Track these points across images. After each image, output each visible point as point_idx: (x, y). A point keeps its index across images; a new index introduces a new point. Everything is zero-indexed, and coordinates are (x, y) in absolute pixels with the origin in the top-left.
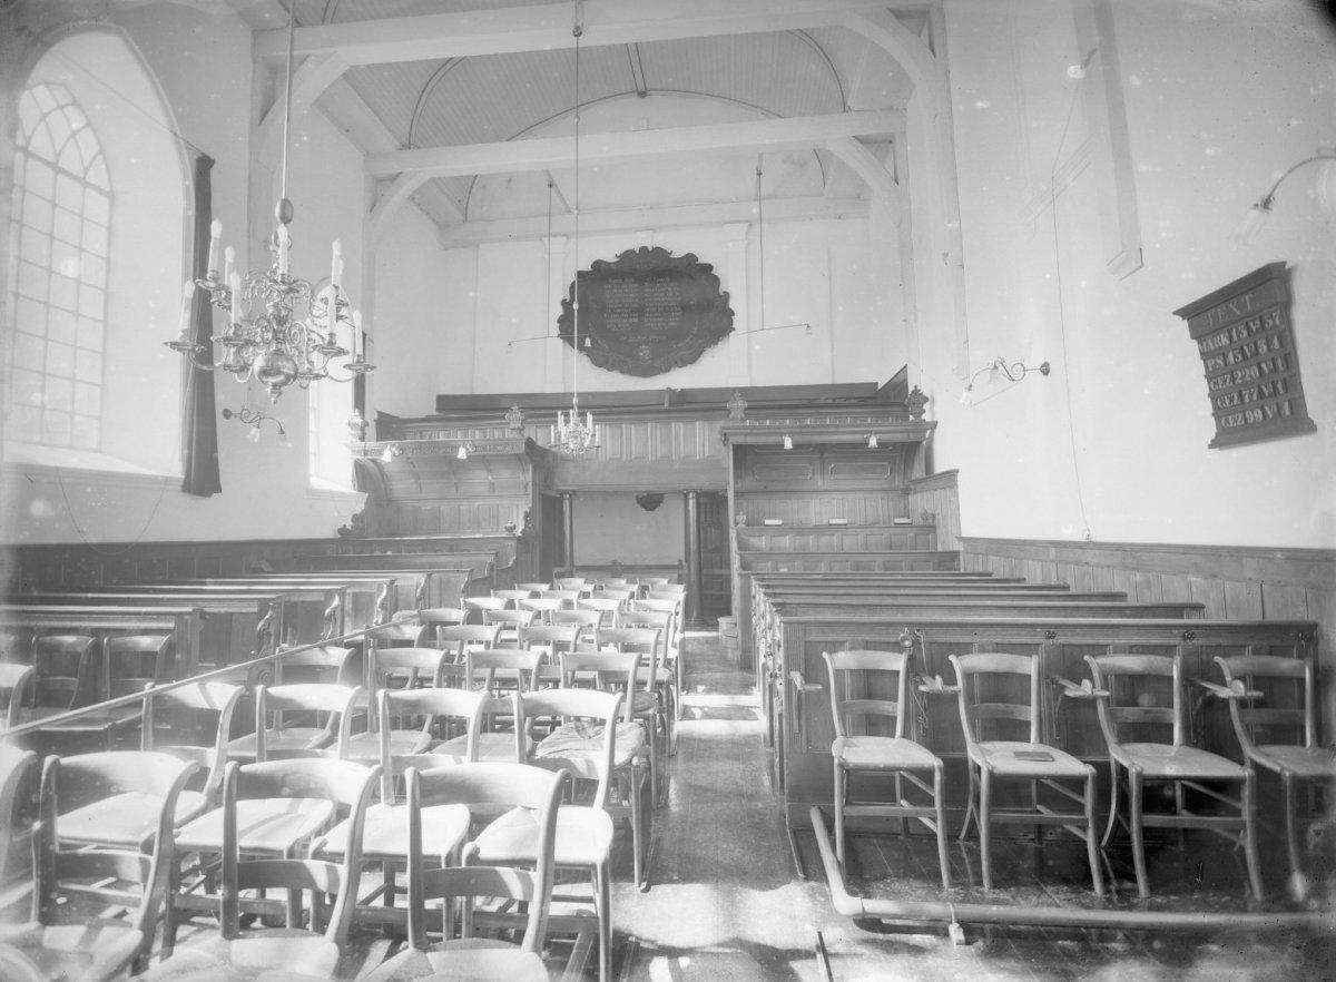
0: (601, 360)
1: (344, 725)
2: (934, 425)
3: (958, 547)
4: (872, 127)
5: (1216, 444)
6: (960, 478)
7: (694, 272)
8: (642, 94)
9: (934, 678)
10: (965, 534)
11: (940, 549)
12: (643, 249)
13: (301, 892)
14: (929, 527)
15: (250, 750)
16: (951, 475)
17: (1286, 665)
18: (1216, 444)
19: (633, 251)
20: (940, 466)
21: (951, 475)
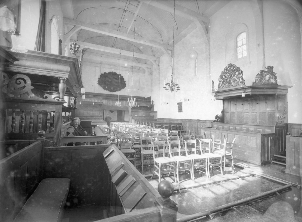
0: (105, 88)
1: (164, 155)
2: (154, 105)
3: (157, 119)
4: (149, 67)
5: (178, 112)
6: (158, 112)
7: (122, 79)
8: (113, 47)
9: (85, 92)
10: (158, 118)
11: (154, 119)
12: (113, 72)
13: (275, 132)
14: (153, 117)
15: (231, 151)
16: (156, 112)
17: (180, 126)
18: (178, 112)
19: (111, 72)
20: (155, 110)
21: (156, 112)
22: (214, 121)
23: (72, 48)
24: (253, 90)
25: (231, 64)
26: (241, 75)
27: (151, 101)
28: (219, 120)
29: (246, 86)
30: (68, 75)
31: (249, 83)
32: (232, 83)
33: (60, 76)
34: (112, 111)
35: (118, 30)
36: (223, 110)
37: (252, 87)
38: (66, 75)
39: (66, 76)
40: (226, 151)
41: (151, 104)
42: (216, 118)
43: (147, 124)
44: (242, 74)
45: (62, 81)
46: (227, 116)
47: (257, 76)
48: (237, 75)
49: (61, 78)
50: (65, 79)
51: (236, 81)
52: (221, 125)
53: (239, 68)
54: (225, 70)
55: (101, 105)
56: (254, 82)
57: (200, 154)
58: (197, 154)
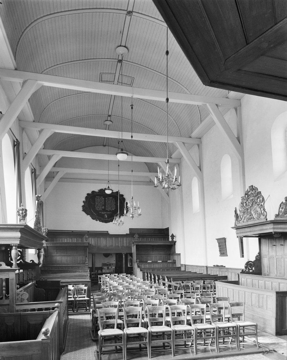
10: (181, 263)
16: (179, 254)
22: (243, 272)
23: (19, 215)
24: (276, 226)
25: (252, 186)
26: (262, 204)
27: (170, 235)
28: (252, 269)
29: (268, 220)
30: (19, 241)
31: (271, 217)
32: (253, 215)
33: (12, 243)
34: (107, 255)
35: (113, 98)
36: (258, 253)
37: (273, 222)
38: (17, 241)
39: (18, 242)
40: (233, 318)
41: (170, 240)
42: (246, 268)
43: (158, 277)
44: (263, 202)
45: (14, 248)
46: (265, 262)
47: (281, 206)
48: (258, 203)
49: (13, 245)
50: (17, 245)
51: (258, 213)
52: (255, 279)
53: (260, 193)
54: (246, 194)
55: (89, 246)
56: (277, 215)
57: (190, 325)
58: (141, 327)
